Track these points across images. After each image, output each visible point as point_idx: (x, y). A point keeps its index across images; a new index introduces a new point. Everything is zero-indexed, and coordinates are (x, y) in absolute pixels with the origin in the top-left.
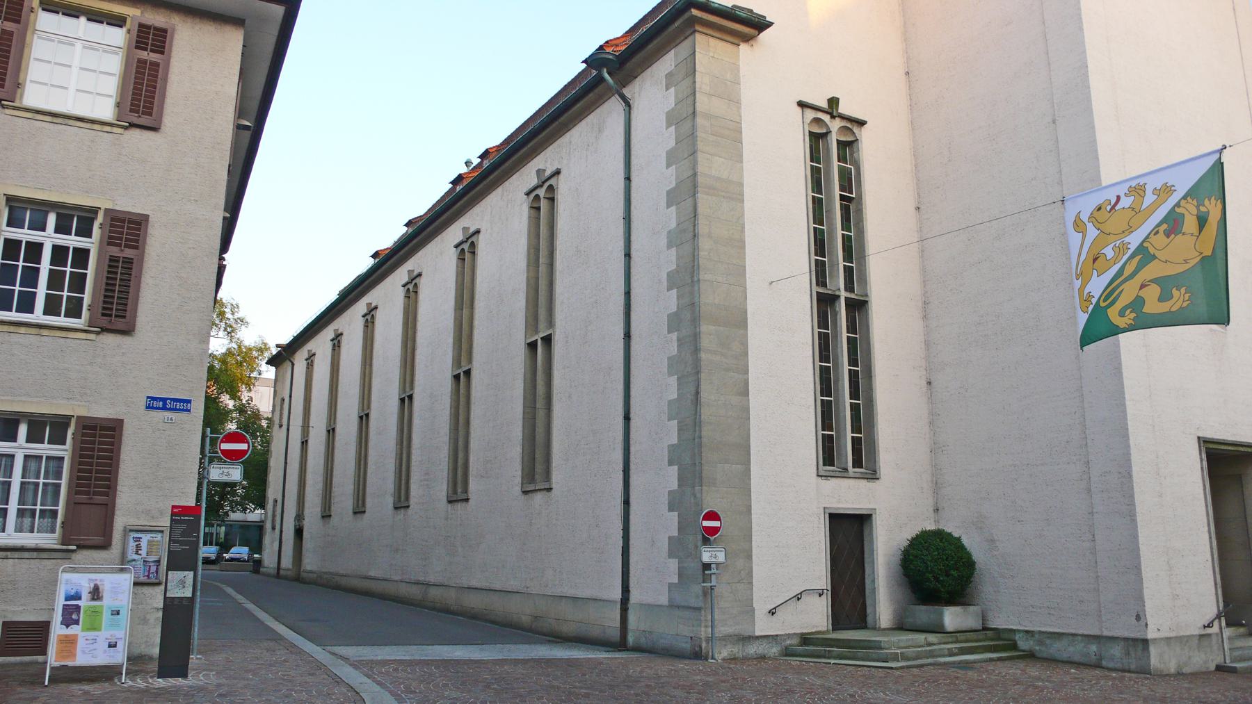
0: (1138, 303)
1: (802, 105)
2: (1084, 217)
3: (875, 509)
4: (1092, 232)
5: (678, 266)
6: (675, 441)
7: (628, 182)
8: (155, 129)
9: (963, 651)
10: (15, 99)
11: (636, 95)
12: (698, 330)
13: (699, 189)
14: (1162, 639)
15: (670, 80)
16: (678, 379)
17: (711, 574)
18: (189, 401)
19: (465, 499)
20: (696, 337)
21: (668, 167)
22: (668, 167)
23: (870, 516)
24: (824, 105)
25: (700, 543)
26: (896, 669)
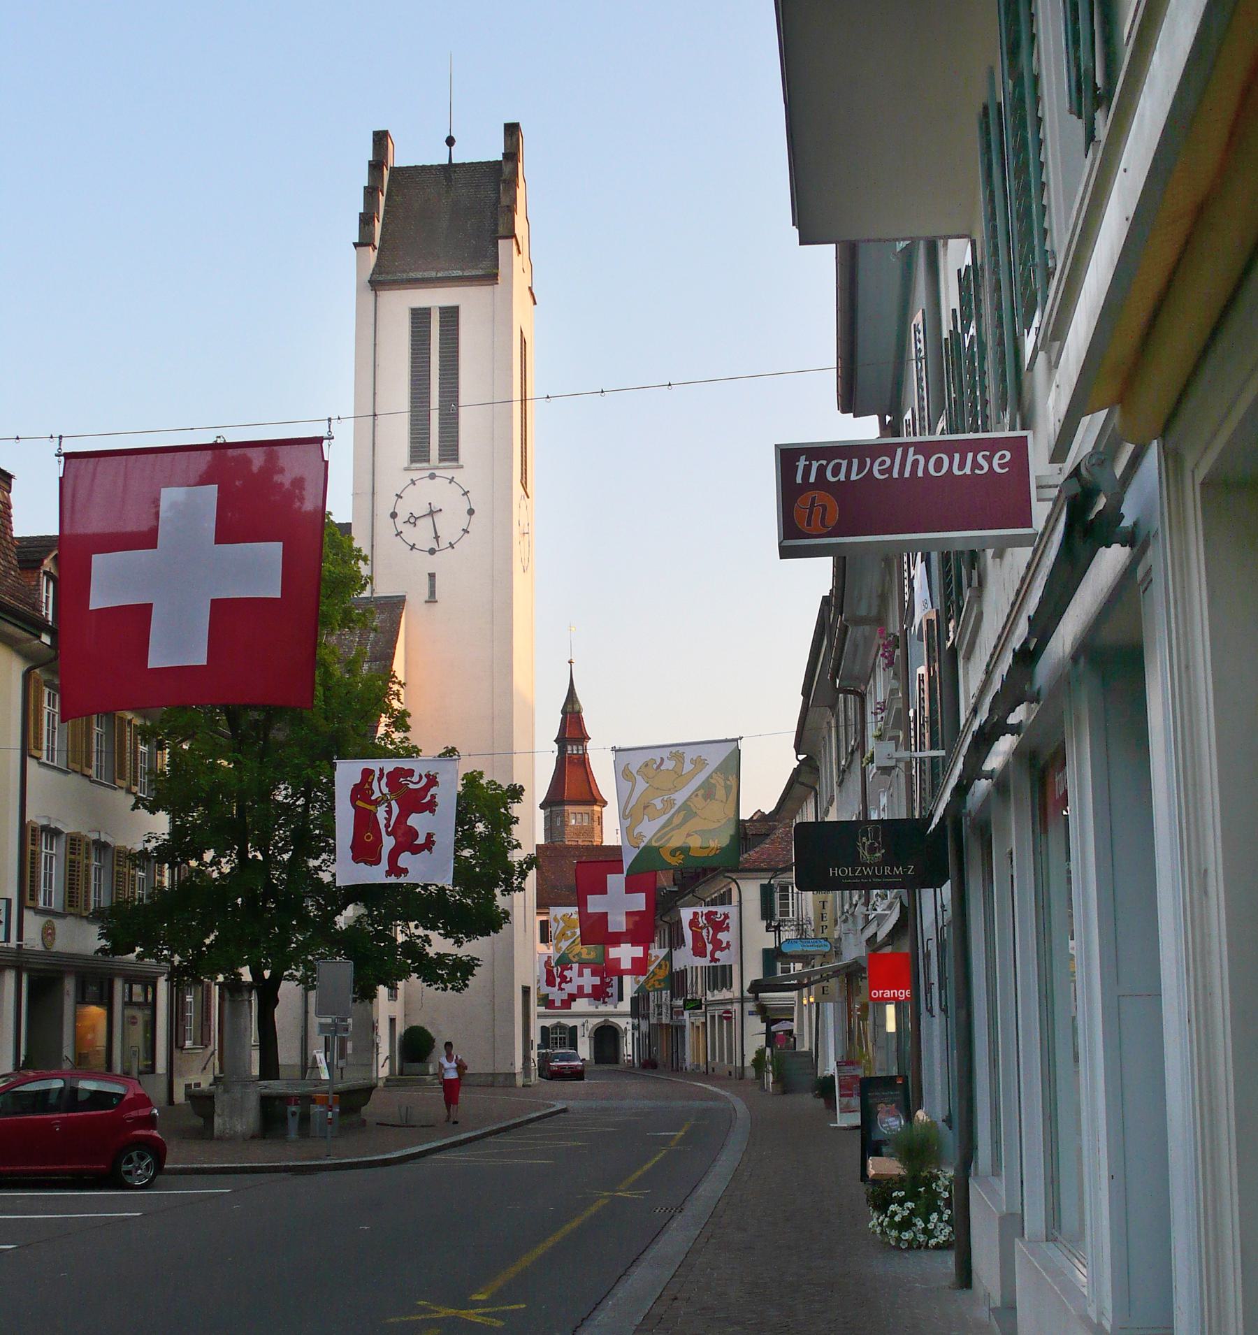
4: (641, 785)
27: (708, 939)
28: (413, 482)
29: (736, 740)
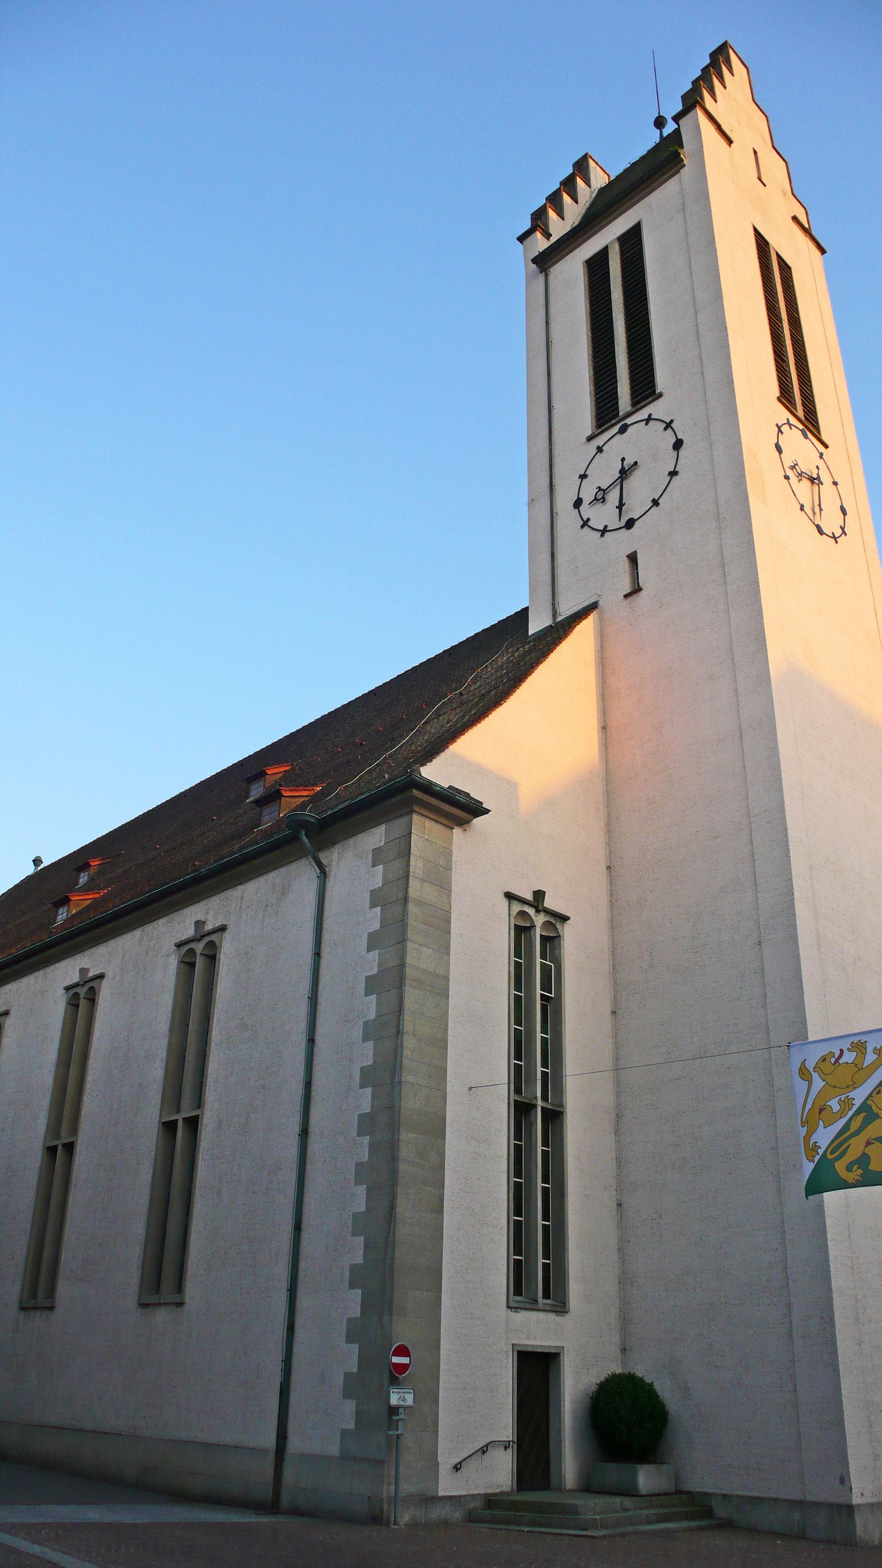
0: (863, 1160)
1: (509, 896)
2: (810, 1066)
3: (563, 1347)
4: (818, 1083)
5: (375, 1061)
6: (359, 1259)
7: (317, 957)
9: (661, 1519)
11: (334, 863)
12: (397, 1137)
13: (407, 981)
14: (865, 1505)
15: (377, 857)
16: (369, 1190)
17: (398, 1421)
19: (50, 1307)
20: (394, 1145)
21: (369, 950)
22: (369, 950)
24: (529, 897)
25: (386, 1382)
26: (600, 1538)
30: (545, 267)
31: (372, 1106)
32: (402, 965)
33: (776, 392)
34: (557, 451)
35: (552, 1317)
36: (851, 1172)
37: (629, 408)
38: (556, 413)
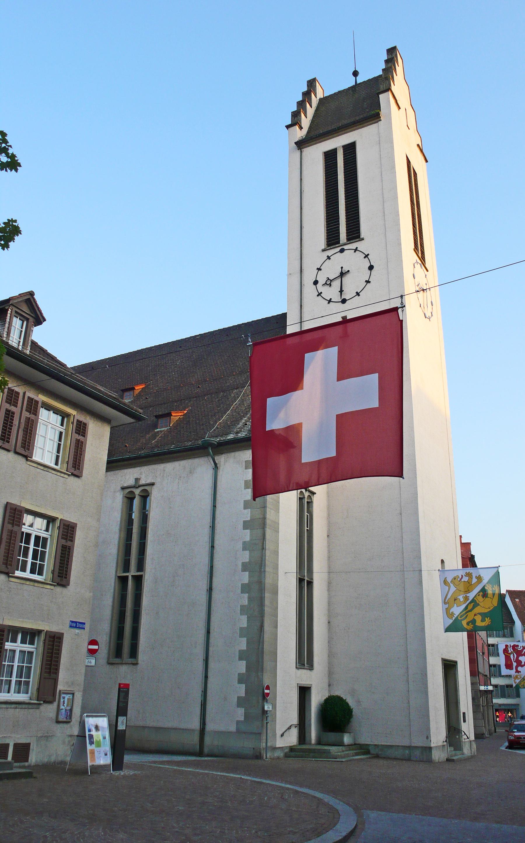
4: (453, 589)
8: (78, 477)
10: (32, 457)
12: (263, 595)
18: (84, 624)
23: (310, 687)
27: (514, 660)
28: (329, 258)
29: (497, 567)
30: (301, 147)
31: (249, 580)
32: (264, 518)
33: (413, 247)
34: (304, 252)
35: (309, 671)
36: (469, 625)
37: (345, 241)
38: (304, 230)
